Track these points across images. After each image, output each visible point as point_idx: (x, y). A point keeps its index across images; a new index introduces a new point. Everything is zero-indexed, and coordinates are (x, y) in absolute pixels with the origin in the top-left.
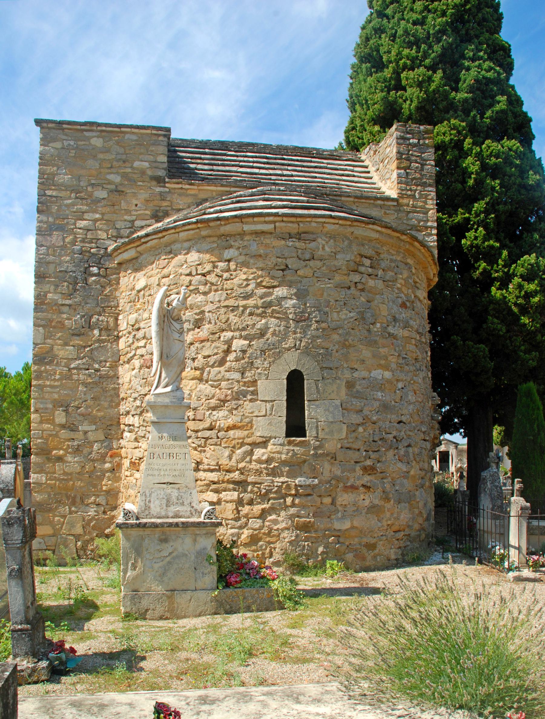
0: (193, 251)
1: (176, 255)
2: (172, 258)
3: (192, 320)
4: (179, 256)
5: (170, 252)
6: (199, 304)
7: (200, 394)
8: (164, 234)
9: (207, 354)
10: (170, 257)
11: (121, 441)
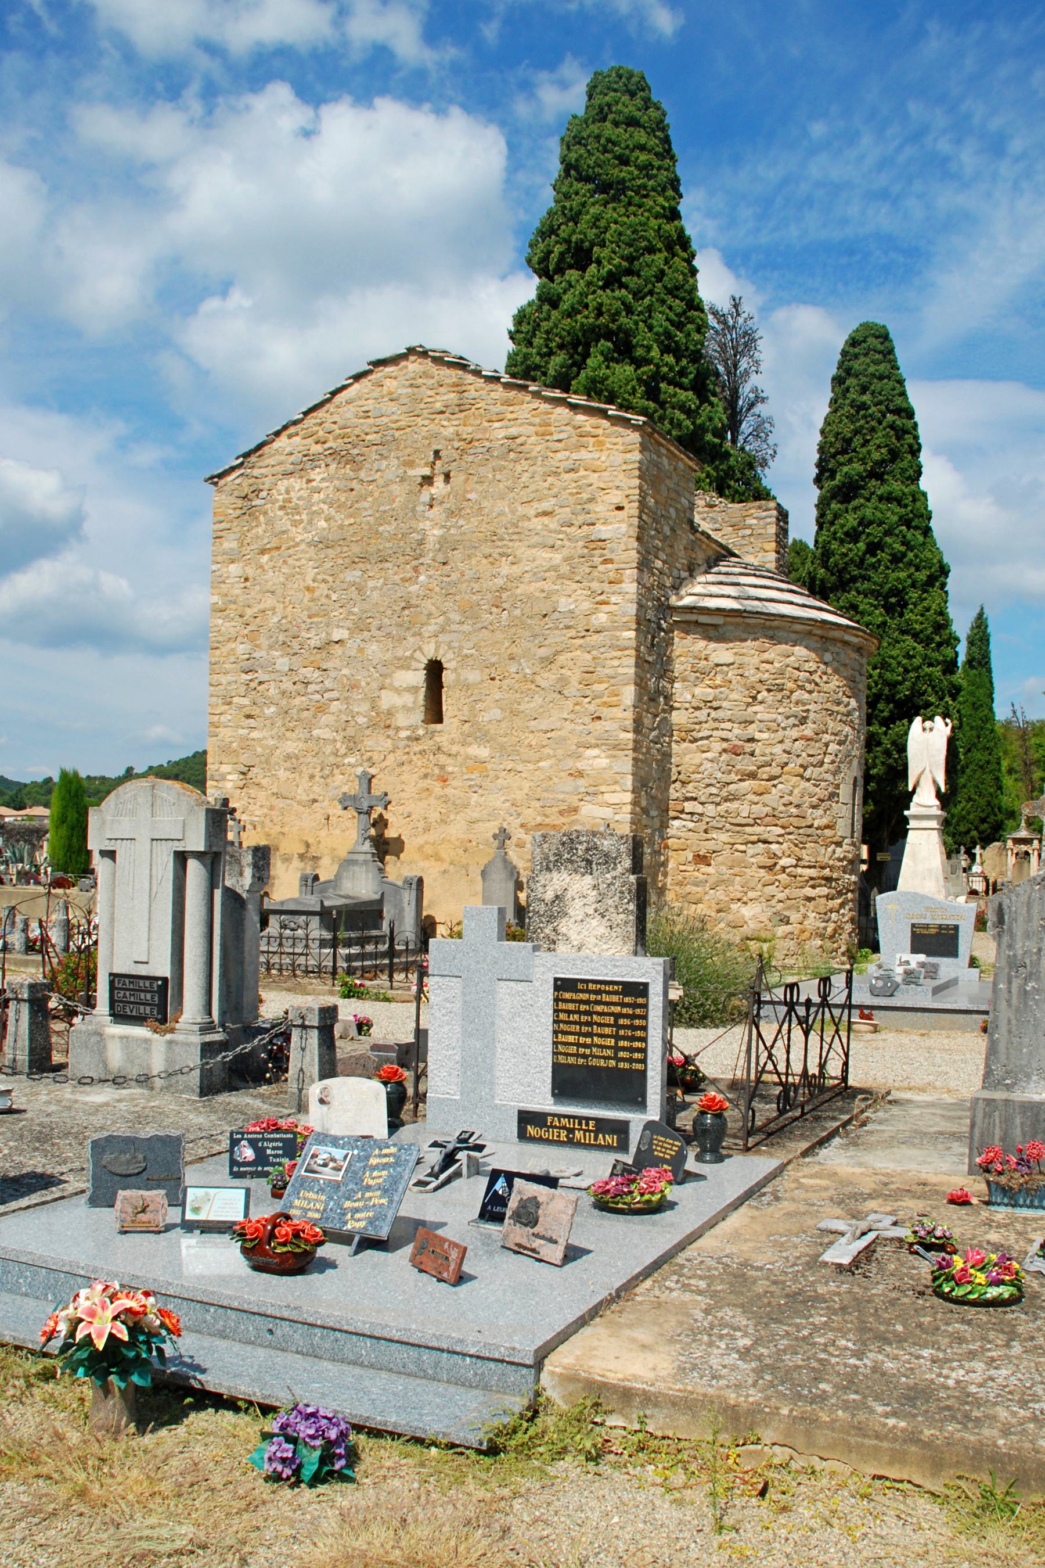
4: (784, 646)
5: (772, 638)
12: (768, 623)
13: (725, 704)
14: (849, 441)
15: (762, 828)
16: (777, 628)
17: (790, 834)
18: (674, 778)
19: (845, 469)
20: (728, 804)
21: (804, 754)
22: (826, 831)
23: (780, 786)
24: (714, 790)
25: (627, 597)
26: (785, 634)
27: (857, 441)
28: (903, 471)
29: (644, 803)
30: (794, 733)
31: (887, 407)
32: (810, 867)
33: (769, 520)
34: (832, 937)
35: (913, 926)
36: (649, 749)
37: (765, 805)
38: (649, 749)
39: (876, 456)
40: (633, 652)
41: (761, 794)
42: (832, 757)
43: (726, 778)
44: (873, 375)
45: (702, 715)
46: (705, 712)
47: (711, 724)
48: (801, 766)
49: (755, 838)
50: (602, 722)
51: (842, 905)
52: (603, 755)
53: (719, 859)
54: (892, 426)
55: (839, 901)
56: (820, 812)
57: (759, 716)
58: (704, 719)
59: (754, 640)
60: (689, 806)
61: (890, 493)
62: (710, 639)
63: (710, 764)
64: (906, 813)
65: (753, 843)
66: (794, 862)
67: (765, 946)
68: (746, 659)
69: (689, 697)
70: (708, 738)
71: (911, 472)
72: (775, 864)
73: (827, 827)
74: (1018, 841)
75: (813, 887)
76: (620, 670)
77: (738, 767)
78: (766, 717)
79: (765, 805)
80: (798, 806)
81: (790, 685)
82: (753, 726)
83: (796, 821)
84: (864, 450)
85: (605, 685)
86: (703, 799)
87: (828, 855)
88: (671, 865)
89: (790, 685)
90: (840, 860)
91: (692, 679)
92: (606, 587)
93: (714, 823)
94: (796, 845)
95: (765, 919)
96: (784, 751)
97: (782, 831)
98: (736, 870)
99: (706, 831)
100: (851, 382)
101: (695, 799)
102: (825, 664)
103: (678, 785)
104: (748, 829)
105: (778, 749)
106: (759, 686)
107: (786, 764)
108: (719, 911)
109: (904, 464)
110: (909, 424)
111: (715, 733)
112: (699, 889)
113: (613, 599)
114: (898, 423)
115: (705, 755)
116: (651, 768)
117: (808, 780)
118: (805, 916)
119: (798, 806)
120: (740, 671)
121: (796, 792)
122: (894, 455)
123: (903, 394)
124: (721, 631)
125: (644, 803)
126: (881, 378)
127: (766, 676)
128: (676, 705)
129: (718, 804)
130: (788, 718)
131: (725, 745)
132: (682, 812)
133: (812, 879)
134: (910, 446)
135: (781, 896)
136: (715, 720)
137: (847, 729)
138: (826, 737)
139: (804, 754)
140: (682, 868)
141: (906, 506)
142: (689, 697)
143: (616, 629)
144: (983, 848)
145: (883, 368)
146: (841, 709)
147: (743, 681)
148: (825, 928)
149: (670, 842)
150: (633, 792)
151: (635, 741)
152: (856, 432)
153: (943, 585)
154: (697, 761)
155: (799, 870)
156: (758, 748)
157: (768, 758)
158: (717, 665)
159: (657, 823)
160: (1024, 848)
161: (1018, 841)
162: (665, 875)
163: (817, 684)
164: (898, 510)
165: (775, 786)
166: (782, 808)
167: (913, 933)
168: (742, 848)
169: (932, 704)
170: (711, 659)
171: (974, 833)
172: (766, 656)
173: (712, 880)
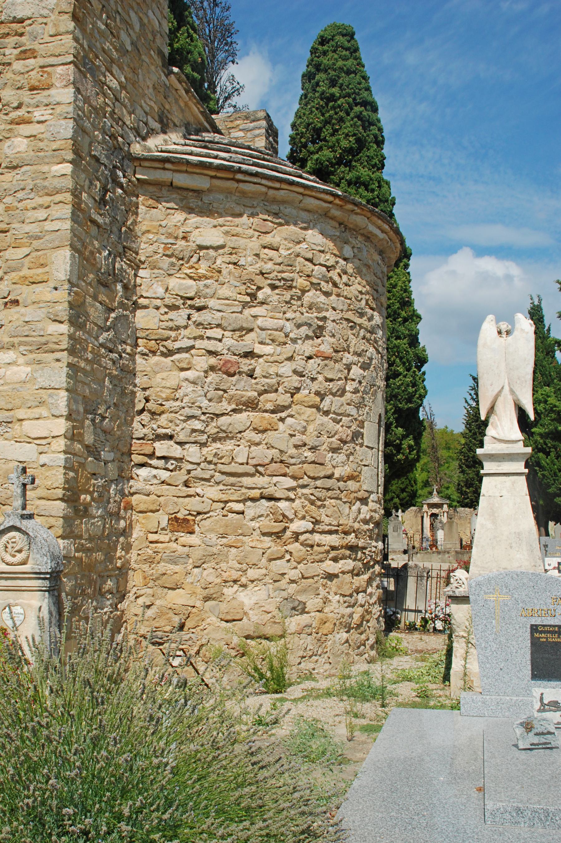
0: (316, 230)
1: (287, 223)
2: (280, 224)
3: (315, 326)
4: (292, 228)
5: (276, 215)
6: (322, 306)
7: (322, 428)
8: (284, 186)
9: (330, 376)
10: (277, 221)
11: (132, 482)
12: (271, 192)
13: (212, 303)
14: (318, 131)
15: (266, 479)
16: (283, 202)
17: (304, 486)
18: (139, 407)
19: (315, 157)
20: (218, 445)
21: (320, 378)
22: (350, 483)
23: (289, 420)
24: (198, 425)
25: (59, 109)
26: (294, 212)
27: (325, 133)
28: (370, 158)
29: (89, 439)
30: (308, 348)
31: (354, 99)
32: (330, 532)
33: (257, 132)
34: (359, 626)
35: (534, 628)
36: (97, 356)
37: (270, 447)
38: (97, 356)
39: (345, 144)
40: (68, 197)
41: (264, 431)
42: (355, 384)
43: (215, 408)
44: (341, 69)
45: (179, 317)
46: (184, 313)
47: (193, 331)
48: (317, 393)
49: (256, 493)
50: (21, 309)
51: (370, 582)
52: (21, 360)
53: (207, 523)
54: (359, 117)
55: (366, 577)
56: (342, 457)
57: (260, 322)
58: (182, 322)
59: (252, 215)
60: (161, 448)
61: (358, 178)
62: (190, 210)
63: (191, 388)
64: (479, 451)
65: (253, 500)
66: (310, 526)
67: (273, 647)
68: (241, 242)
69: (160, 291)
70: (188, 349)
71: (376, 161)
72: (285, 529)
73: (351, 478)
74: (431, 506)
75: (335, 560)
76: (49, 226)
77: (231, 392)
78: (270, 323)
79: (270, 447)
80: (313, 449)
81: (301, 282)
82: (252, 335)
83: (311, 470)
84: (334, 139)
85: (26, 251)
86: (182, 437)
87: (352, 516)
88: (136, 533)
89: (301, 282)
90: (366, 522)
91: (165, 266)
92: (26, 96)
93: (198, 473)
94: (312, 503)
95: (271, 608)
96: (295, 372)
97: (293, 483)
98: (231, 539)
99: (186, 484)
100: (320, 76)
101: (171, 437)
102: (345, 259)
103: (146, 417)
104: (247, 481)
105: (286, 369)
106: (260, 281)
107: (298, 389)
108: (207, 599)
109: (371, 153)
110: (373, 116)
111: (199, 344)
112: (177, 568)
113: (37, 115)
114: (365, 113)
115: (184, 374)
116: (103, 386)
117: (326, 413)
118: (326, 601)
119: (313, 449)
120: (234, 258)
121: (311, 428)
122: (361, 143)
123: (368, 89)
124: (206, 199)
125: (89, 439)
126: (348, 72)
127: (269, 266)
128: (141, 301)
129: (203, 445)
130: (299, 326)
131: (213, 361)
132: (152, 455)
133: (333, 548)
134: (376, 137)
135: (294, 574)
136: (198, 325)
137: (372, 350)
138: (348, 358)
139: (320, 378)
140: (152, 537)
141: (373, 191)
142: (160, 291)
143: (42, 161)
144: (403, 511)
145: (349, 63)
146: (363, 321)
147: (237, 272)
148: (351, 616)
149: (135, 500)
150: (69, 417)
151: (71, 337)
152: (327, 122)
153: (406, 266)
154: (173, 383)
155: (317, 537)
156: (260, 367)
157: (274, 381)
158: (201, 248)
159: (112, 470)
160: (435, 511)
161: (431, 506)
162: (128, 548)
163: (335, 285)
164: (365, 193)
165: (282, 420)
166: (293, 451)
167: (535, 644)
168: (238, 507)
169: (400, 374)
170: (192, 238)
171: (396, 500)
172: (268, 239)
173: (197, 554)
